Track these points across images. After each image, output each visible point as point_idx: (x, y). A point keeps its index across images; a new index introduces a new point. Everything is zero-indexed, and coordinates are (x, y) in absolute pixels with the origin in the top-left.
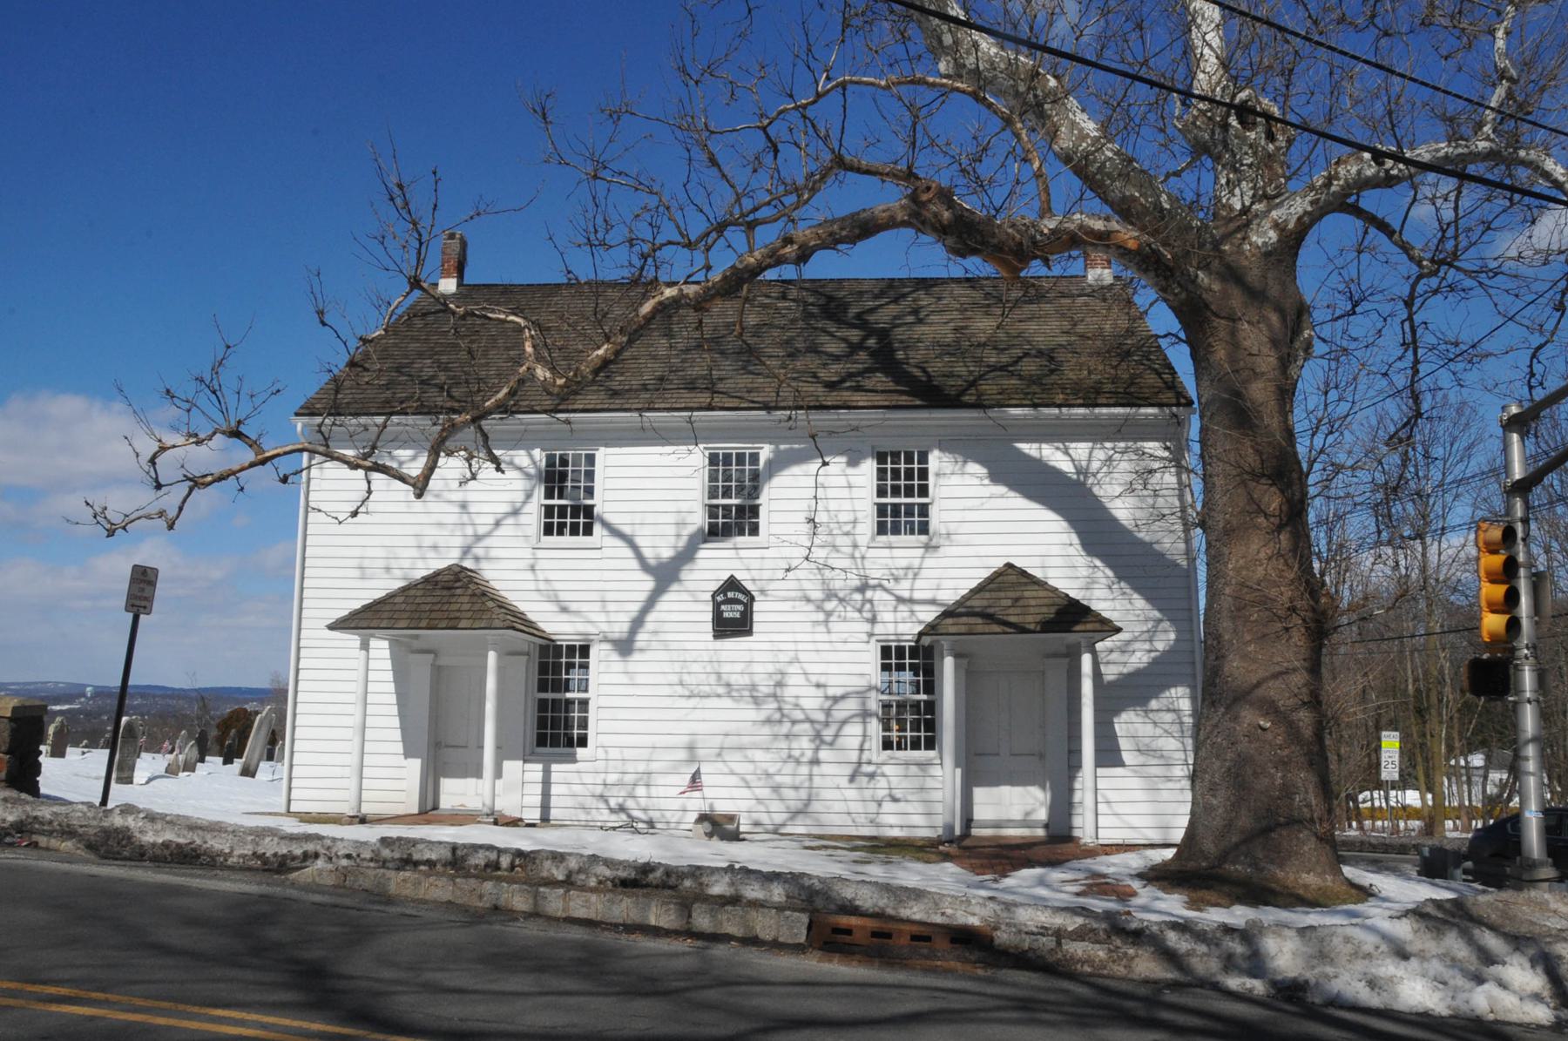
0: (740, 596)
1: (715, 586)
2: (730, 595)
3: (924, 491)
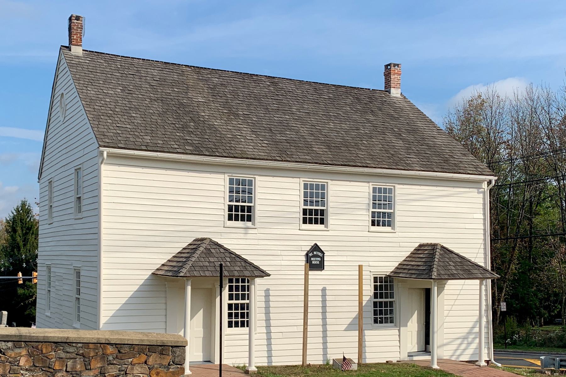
0: (320, 254)
1: (308, 248)
2: (315, 253)
3: (305, 211)
